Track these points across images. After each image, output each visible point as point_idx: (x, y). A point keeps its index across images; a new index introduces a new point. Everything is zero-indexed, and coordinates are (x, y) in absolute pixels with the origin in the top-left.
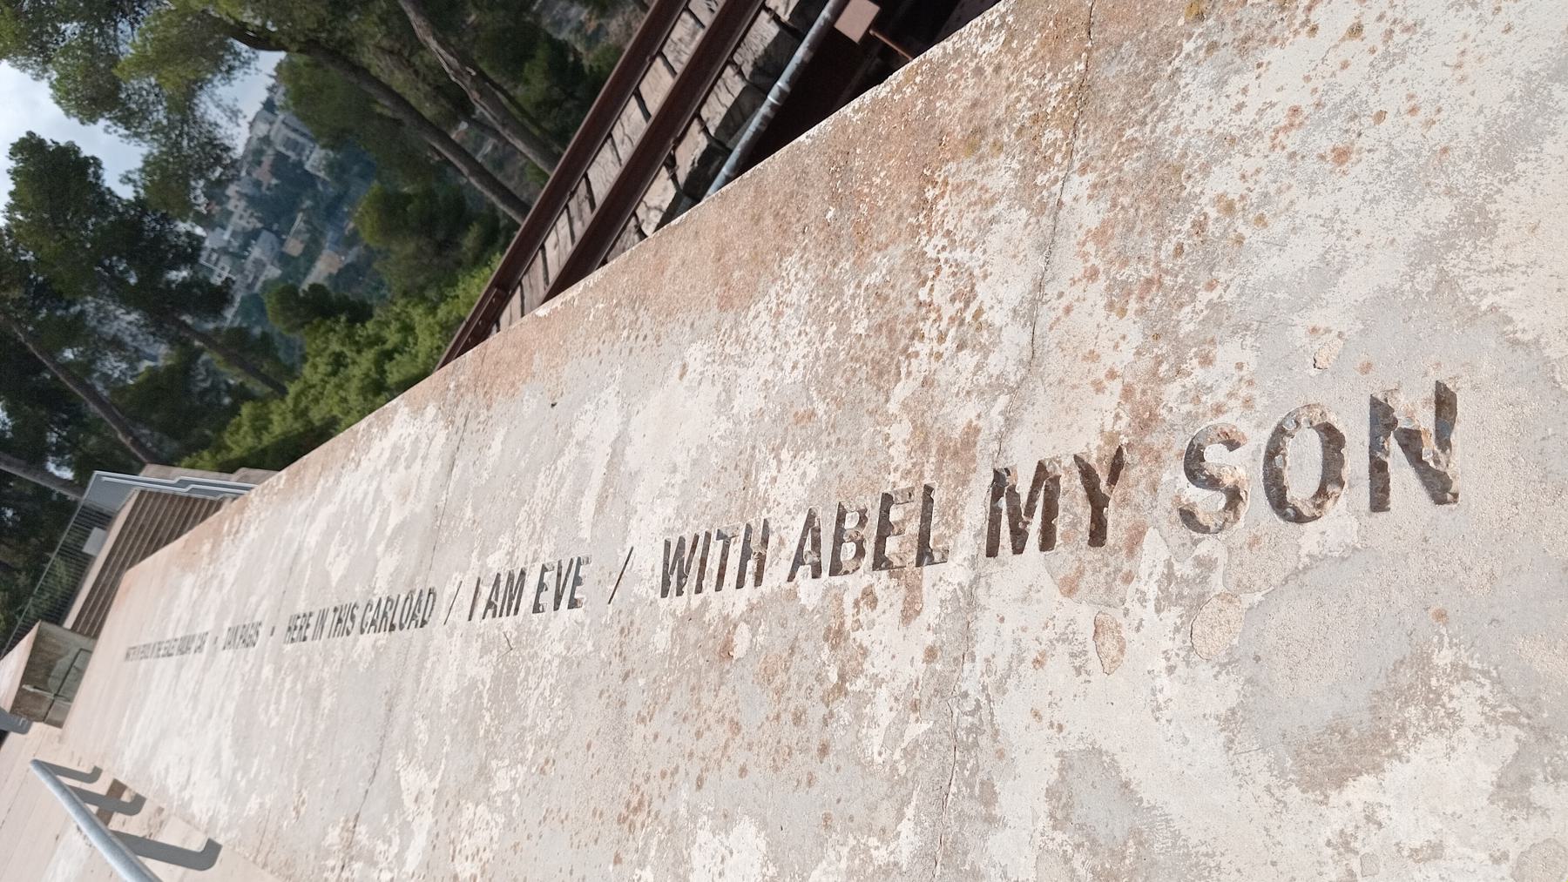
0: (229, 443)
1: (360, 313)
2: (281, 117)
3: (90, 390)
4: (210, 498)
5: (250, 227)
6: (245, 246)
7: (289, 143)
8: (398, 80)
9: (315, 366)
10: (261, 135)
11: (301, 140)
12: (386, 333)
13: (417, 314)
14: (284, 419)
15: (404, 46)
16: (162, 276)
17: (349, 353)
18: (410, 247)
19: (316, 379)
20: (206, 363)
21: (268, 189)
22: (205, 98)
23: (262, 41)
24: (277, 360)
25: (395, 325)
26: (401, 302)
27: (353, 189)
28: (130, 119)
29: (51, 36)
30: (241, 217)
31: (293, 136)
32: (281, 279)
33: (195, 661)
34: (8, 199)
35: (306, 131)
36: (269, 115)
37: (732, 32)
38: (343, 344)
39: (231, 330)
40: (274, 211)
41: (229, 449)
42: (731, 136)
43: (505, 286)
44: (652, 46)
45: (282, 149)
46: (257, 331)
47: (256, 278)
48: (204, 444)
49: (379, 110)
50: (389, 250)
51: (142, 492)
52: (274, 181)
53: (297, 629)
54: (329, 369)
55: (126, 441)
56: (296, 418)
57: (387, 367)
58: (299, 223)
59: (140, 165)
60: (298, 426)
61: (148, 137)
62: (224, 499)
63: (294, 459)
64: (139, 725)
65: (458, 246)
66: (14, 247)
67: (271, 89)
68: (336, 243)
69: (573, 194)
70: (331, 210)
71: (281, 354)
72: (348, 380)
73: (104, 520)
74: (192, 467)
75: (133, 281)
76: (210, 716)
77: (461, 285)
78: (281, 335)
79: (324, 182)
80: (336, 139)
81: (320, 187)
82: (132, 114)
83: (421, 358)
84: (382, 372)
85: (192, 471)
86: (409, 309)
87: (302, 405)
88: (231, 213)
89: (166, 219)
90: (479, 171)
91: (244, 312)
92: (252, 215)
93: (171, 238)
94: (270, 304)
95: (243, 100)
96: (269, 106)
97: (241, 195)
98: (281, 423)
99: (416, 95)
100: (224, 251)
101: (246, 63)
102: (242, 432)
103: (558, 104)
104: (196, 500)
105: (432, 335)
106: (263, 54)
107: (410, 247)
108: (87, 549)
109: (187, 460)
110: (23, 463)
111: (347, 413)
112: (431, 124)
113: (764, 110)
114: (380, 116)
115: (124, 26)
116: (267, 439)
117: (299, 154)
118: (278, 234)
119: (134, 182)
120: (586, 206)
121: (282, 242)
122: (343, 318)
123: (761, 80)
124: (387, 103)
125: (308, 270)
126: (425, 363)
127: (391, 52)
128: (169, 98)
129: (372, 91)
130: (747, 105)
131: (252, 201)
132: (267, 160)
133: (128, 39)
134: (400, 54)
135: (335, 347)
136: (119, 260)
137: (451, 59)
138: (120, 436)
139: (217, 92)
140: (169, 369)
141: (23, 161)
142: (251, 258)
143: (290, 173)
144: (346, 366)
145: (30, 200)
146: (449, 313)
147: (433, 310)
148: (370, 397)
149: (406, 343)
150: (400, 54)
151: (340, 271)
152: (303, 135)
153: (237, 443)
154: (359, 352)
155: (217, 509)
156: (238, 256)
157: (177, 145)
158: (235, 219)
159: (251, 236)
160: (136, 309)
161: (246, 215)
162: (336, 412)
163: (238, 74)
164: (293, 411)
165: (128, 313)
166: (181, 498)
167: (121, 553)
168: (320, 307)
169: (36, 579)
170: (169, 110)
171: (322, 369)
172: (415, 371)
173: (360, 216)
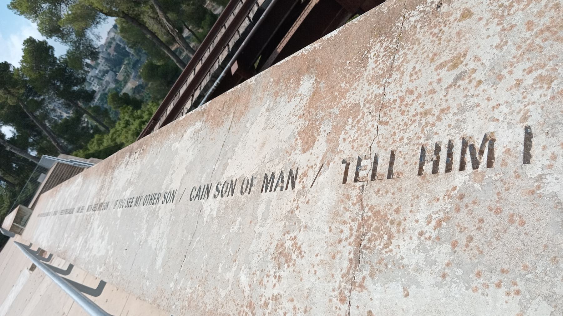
3: (44, 126)
5: (105, 69)
9: (119, 124)
12: (144, 115)
16: (71, 89)
17: (131, 121)
19: (119, 128)
23: (110, 14)
24: (110, 118)
25: (147, 113)
28: (63, 37)
29: (39, 8)
30: (103, 65)
33: (48, 217)
34: (21, 58)
36: (114, 30)
37: (211, 63)
38: (130, 117)
40: (114, 64)
41: (89, 150)
44: (199, 57)
45: (119, 42)
47: (106, 87)
48: (81, 147)
51: (58, 163)
52: (115, 54)
53: (61, 213)
54: (124, 125)
55: (55, 144)
59: (66, 53)
60: (112, 144)
61: (69, 43)
66: (23, 74)
73: (45, 170)
74: (76, 155)
79: (133, 55)
81: (131, 57)
85: (75, 157)
87: (114, 137)
88: (99, 64)
92: (106, 65)
93: (76, 75)
95: (103, 31)
97: (103, 58)
98: (107, 142)
100: (96, 77)
104: (76, 167)
106: (110, 17)
108: (39, 180)
109: (74, 153)
110: (20, 149)
112: (164, 44)
113: (213, 87)
115: (63, 6)
116: (102, 148)
118: (115, 72)
121: (116, 75)
123: (213, 79)
127: (153, 18)
130: (209, 85)
131: (107, 60)
132: (113, 46)
133: (65, 11)
135: (127, 118)
136: (58, 81)
137: (170, 26)
138: (53, 142)
141: (28, 46)
142: (105, 80)
144: (129, 125)
145: (29, 60)
151: (136, 87)
153: (92, 148)
154: (134, 120)
155: (82, 171)
158: (100, 66)
160: (63, 98)
161: (104, 65)
164: (111, 139)
165: (59, 100)
166: (71, 166)
169: (21, 189)
171: (122, 125)
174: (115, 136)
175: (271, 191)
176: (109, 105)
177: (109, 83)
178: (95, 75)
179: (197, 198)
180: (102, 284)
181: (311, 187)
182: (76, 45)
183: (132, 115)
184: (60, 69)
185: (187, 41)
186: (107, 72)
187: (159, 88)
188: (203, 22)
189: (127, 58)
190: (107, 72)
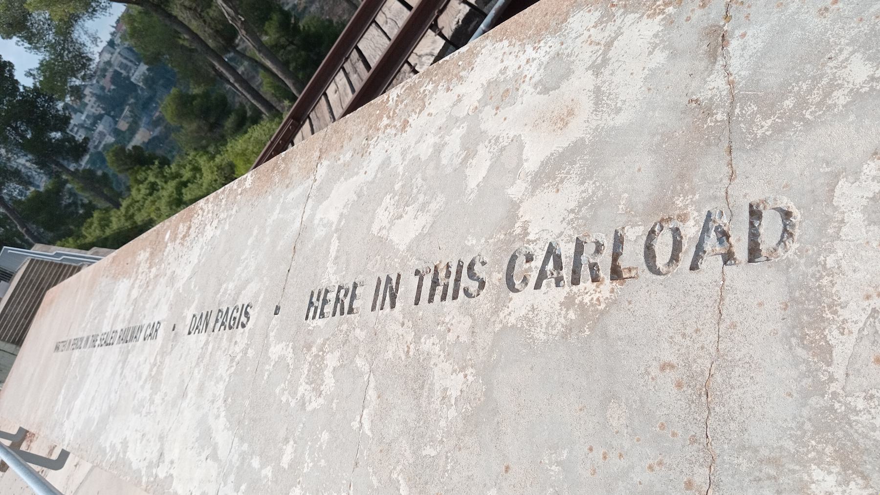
0: (84, 233)
1: (165, 162)
2: (118, 50)
4: (74, 264)
5: (97, 113)
6: (94, 124)
7: (122, 65)
8: (194, 25)
9: (139, 190)
10: (106, 60)
11: (129, 64)
12: (183, 171)
13: (202, 161)
14: (119, 220)
15: (198, 5)
18: (194, 126)
19: (139, 197)
20: (69, 189)
21: (109, 91)
22: (77, 27)
24: (111, 188)
25: (188, 167)
26: (192, 153)
27: (159, 93)
28: (32, 38)
30: (92, 107)
31: (125, 61)
32: (116, 142)
35: (133, 59)
38: (157, 177)
39: (84, 170)
42: (486, 4)
43: (299, 118)
45: (118, 69)
46: (99, 173)
47: (100, 142)
48: (70, 234)
49: (181, 42)
50: (182, 127)
51: (32, 260)
52: (113, 87)
54: (148, 191)
56: (127, 220)
57: (184, 191)
58: (126, 111)
59: (38, 66)
60: (128, 224)
62: (83, 265)
63: (124, 244)
64: (78, 403)
65: (223, 126)
67: (112, 34)
68: (148, 124)
69: (347, 59)
70: (146, 105)
71: (114, 185)
72: (159, 198)
75: (29, 136)
76: (184, 395)
77: (229, 145)
78: (115, 175)
79: (142, 89)
80: (153, 61)
81: (140, 92)
82: (33, 35)
83: (205, 186)
84: (180, 194)
85: (63, 248)
86: (197, 158)
87: (130, 213)
88: (87, 104)
89: (51, 99)
90: (240, 79)
91: (92, 161)
93: (53, 112)
94: (109, 158)
96: (111, 43)
97: (93, 94)
98: (117, 222)
99: (205, 33)
100: (81, 126)
101: (105, 9)
102: (93, 227)
103: (284, 47)
104: (65, 265)
105: (212, 172)
107: (194, 126)
111: (159, 217)
114: (182, 46)
116: (108, 232)
117: (128, 72)
118: (113, 117)
119: (34, 75)
120: (361, 66)
121: (116, 123)
122: (157, 163)
124: (186, 37)
125: (131, 139)
126: (207, 189)
127: (190, 9)
128: (56, 27)
129: (179, 30)
131: (99, 98)
132: (109, 75)
134: (195, 10)
135: (151, 179)
137: (230, 10)
139: (86, 25)
140: (47, 191)
142: (97, 131)
143: (122, 82)
144: (158, 190)
146: (223, 160)
147: (213, 158)
148: (174, 207)
149: (195, 177)
150: (195, 10)
151: (150, 141)
152: (131, 61)
153: (90, 234)
154: (166, 182)
156: (90, 129)
157: (62, 56)
158: (88, 108)
159: (98, 118)
160: (31, 153)
161: (95, 106)
162: (153, 216)
163: (97, 15)
164: (125, 216)
166: (56, 264)
167: (18, 297)
168: (140, 159)
170: (56, 34)
171: (143, 191)
172: (201, 194)
173: (165, 106)
174: (131, 211)
175: (444, 298)
176: (112, 168)
177: (105, 135)
178: (81, 122)
179: (223, 327)
180: (64, 455)
181: (416, 304)
182: (55, 50)
183: (161, 172)
184: (26, 101)
185: (232, 64)
186: (100, 117)
187: (196, 135)
188: (267, 23)
189: (134, 94)
190: (100, 117)
